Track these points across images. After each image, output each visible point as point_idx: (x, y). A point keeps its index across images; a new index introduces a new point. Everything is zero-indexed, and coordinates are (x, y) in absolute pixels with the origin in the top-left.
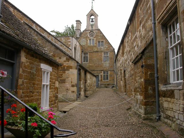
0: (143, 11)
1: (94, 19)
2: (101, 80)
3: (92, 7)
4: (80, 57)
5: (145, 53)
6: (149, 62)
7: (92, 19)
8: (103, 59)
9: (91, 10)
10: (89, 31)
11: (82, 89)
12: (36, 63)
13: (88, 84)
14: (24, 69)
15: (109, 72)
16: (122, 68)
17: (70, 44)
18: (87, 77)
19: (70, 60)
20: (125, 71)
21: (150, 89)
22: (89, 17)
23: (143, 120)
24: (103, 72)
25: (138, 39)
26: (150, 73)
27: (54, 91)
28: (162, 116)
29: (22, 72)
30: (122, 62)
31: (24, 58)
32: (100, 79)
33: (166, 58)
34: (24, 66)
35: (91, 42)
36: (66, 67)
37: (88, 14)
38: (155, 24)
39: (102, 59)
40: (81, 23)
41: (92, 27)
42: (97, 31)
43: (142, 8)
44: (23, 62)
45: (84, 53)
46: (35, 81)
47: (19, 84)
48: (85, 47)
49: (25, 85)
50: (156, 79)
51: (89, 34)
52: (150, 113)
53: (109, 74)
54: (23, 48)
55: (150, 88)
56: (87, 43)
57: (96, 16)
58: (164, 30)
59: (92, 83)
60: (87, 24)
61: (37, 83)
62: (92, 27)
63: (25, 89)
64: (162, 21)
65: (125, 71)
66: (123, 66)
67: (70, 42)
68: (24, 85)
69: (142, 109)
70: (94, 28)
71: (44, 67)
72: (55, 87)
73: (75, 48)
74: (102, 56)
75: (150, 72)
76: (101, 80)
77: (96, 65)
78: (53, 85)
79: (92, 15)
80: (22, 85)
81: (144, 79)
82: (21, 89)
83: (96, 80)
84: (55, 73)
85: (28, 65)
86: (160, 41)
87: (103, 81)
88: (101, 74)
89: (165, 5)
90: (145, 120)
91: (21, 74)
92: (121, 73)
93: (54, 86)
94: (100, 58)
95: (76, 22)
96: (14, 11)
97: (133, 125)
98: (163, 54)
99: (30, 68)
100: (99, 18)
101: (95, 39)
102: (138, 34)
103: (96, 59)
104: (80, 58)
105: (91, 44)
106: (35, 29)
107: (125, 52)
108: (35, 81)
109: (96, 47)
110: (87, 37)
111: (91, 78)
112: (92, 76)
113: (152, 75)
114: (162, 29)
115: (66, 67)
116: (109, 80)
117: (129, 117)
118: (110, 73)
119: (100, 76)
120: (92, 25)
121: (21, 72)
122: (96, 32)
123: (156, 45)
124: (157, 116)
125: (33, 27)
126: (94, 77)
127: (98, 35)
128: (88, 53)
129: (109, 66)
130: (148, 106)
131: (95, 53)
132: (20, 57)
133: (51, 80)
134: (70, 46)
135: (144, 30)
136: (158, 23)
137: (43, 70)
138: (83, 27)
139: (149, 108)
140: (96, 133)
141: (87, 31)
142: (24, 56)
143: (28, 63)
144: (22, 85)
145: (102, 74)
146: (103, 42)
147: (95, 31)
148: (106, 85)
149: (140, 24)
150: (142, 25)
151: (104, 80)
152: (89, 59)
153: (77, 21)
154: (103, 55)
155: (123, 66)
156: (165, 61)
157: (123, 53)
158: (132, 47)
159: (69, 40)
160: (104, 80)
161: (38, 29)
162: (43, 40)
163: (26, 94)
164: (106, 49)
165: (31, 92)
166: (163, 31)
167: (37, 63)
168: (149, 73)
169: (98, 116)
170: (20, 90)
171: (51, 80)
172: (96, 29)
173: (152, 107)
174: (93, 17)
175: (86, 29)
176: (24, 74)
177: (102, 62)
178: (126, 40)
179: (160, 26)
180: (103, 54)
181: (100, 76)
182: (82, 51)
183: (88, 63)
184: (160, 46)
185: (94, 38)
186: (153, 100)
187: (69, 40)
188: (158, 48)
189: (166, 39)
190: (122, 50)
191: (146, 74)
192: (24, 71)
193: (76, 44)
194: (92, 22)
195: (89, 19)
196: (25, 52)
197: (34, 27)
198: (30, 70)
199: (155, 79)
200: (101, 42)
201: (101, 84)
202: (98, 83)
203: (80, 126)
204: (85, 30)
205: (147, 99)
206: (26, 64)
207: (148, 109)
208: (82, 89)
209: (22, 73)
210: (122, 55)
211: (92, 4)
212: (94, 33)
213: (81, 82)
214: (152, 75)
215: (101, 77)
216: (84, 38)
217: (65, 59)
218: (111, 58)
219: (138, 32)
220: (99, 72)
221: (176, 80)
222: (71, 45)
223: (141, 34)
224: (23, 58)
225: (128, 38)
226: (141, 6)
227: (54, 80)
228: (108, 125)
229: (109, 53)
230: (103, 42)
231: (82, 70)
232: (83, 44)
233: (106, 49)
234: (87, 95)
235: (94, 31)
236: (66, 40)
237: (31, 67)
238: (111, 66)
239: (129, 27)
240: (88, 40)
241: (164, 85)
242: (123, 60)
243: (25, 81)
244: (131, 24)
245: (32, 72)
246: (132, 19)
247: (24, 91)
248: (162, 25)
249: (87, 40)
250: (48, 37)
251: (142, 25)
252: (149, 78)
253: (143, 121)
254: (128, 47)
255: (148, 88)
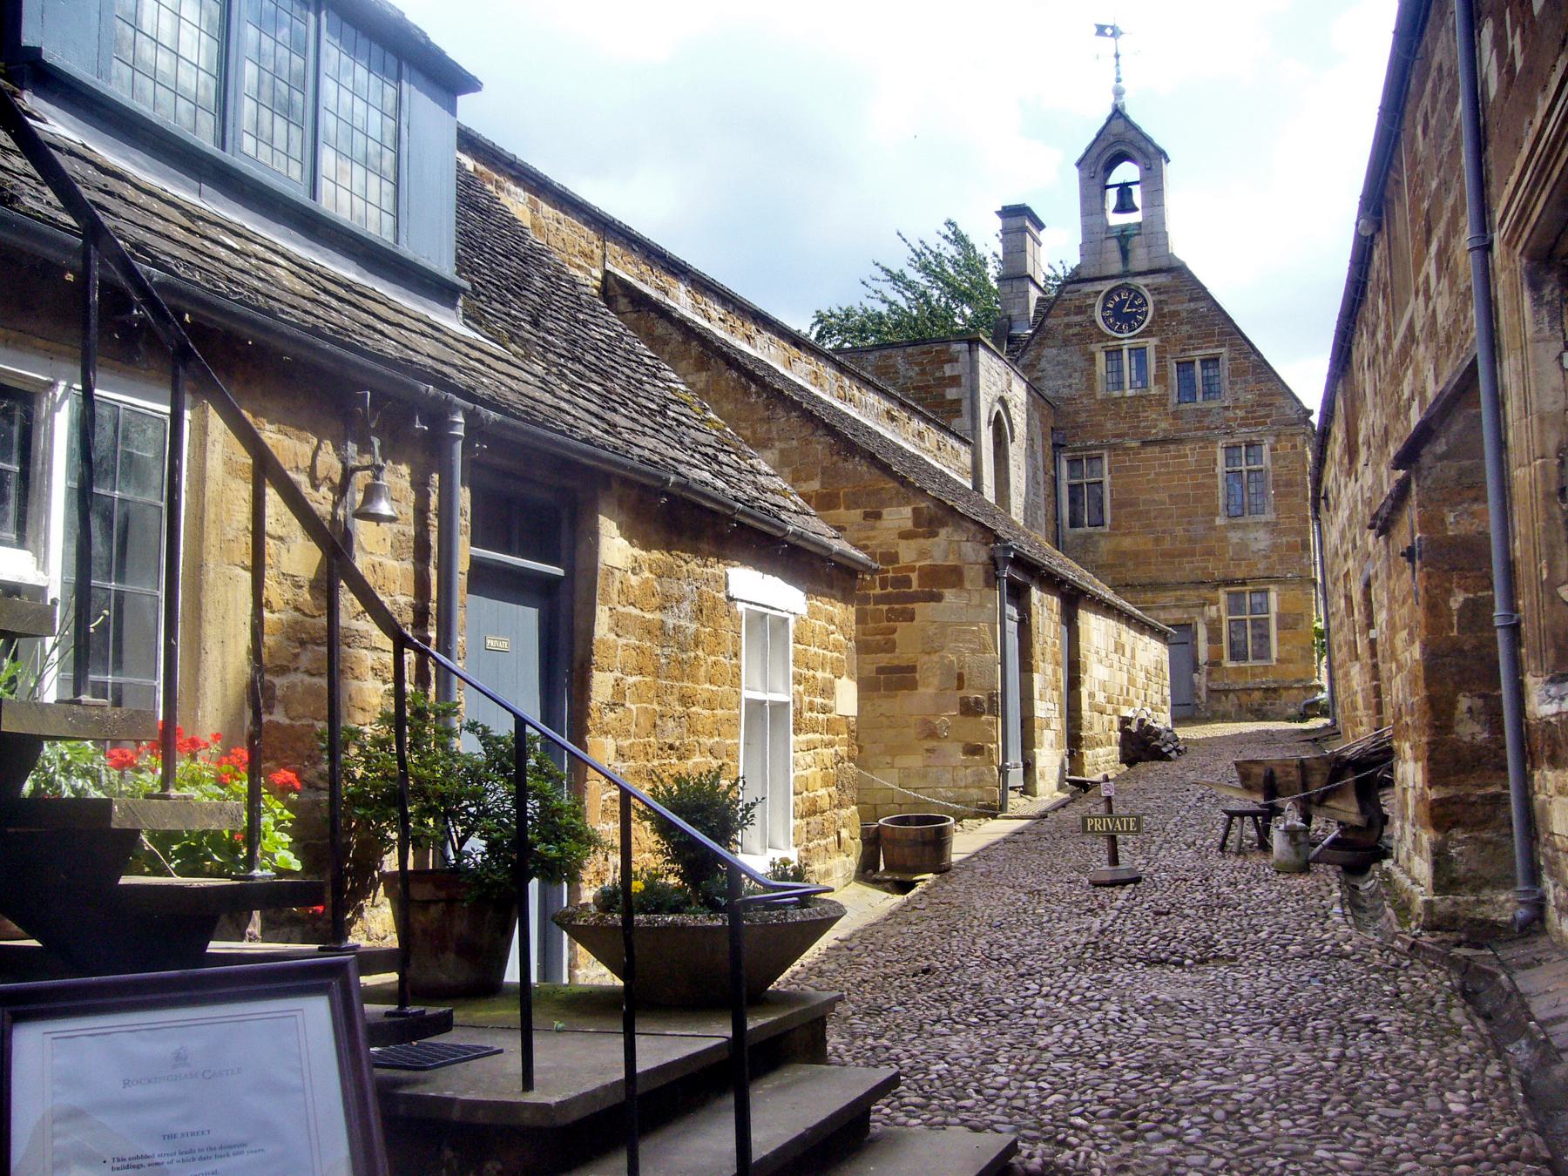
0: (1438, 147)
1: (1136, 191)
2: (1215, 663)
3: (1119, 80)
4: (1042, 492)
5: (1426, 459)
6: (1455, 523)
7: (1124, 189)
8: (1221, 493)
9: (1110, 120)
10: (1098, 286)
11: (1048, 727)
12: (692, 565)
13: (1091, 695)
14: (620, 608)
15: (1273, 596)
16: (1350, 563)
17: (959, 401)
18: (1089, 641)
19: (944, 525)
20: (1368, 585)
21: (1470, 710)
22: (1101, 174)
23: (1424, 928)
24: (1222, 595)
25: (1422, 348)
26: (1466, 600)
27: (830, 744)
28: (1551, 896)
29: (611, 630)
30: (1350, 518)
31: (622, 543)
32: (1203, 656)
33: (1562, 491)
34: (621, 592)
35: (1120, 371)
36: (914, 576)
37: (1088, 150)
38: (1488, 248)
39: (1213, 497)
40: (1040, 226)
41: (1125, 254)
42: (1160, 279)
43: (1433, 122)
44: (611, 570)
45: (1071, 462)
46: (693, 678)
47: (593, 704)
48: (1077, 413)
49: (633, 707)
50: (1501, 637)
51: (1105, 308)
52: (1478, 883)
53: (1274, 607)
54: (608, 486)
55: (1464, 703)
56: (1090, 376)
57: (1151, 157)
58: (1547, 291)
59: (1132, 682)
60: (1087, 231)
61: (705, 695)
62: (1125, 254)
63: (633, 729)
64: (1525, 235)
65: (1368, 585)
66: (1354, 546)
67: (955, 381)
68: (628, 704)
69: (1425, 855)
70: (1139, 260)
71: (753, 586)
72: (832, 715)
73: (997, 424)
74: (1215, 476)
75: (1466, 590)
76: (1215, 663)
77: (1167, 544)
78: (818, 700)
79: (1120, 158)
80: (612, 706)
81: (1425, 646)
82: (606, 733)
83: (1166, 657)
84: (831, 621)
85: (647, 580)
86: (1523, 373)
87: (1233, 664)
88: (1212, 611)
89: (1526, 124)
90: (1438, 928)
91: (603, 642)
92: (1348, 598)
93: (825, 710)
94: (1198, 486)
95: (997, 224)
96: (534, 210)
97: (1341, 957)
98: (1543, 466)
99: (656, 601)
100: (1171, 174)
101: (1151, 343)
102: (1415, 308)
103: (1164, 496)
104: (1041, 501)
105: (1119, 385)
106: (688, 314)
107: (1360, 440)
108: (693, 678)
109: (1161, 401)
110: (1088, 334)
111: (1119, 648)
112: (1129, 635)
113: (1477, 612)
114: (1535, 286)
115: (914, 576)
116: (1274, 655)
117: (1337, 909)
118: (1281, 603)
119: (1202, 633)
120: (1124, 237)
121: (606, 627)
122: (1156, 290)
123: (1498, 403)
124: (1522, 903)
125: (677, 300)
126: (1146, 639)
127: (1175, 314)
128: (1100, 458)
129: (1275, 547)
130: (1458, 834)
131: (1157, 449)
132: (595, 533)
133: (804, 671)
134: (958, 413)
135: (1445, 282)
136: (1504, 248)
137: (741, 607)
138: (1057, 251)
139: (1461, 842)
140: (1074, 999)
141: (1088, 288)
142: (615, 532)
143: (647, 574)
144: (612, 706)
145: (1219, 609)
146: (1215, 360)
147: (1149, 280)
148: (1257, 695)
149: (1428, 243)
150: (1433, 248)
151: (1233, 657)
152: (1117, 505)
153: (1009, 213)
154: (1221, 468)
155: (1354, 546)
156: (1556, 509)
157: (1351, 450)
158: (1397, 407)
159: (948, 370)
160: (1233, 657)
161: (714, 315)
162: (746, 390)
163: (641, 762)
164: (1240, 413)
165: (671, 747)
166: (1538, 301)
167: (699, 570)
168: (1457, 601)
169: (1119, 904)
170: (602, 739)
171: (804, 671)
172: (1156, 265)
173: (1486, 835)
174: (1126, 172)
175: (1076, 271)
176: (621, 641)
177: (1219, 521)
178: (1363, 348)
179: (1521, 263)
180: (1220, 456)
181: (1202, 633)
182: (1057, 446)
183: (1107, 530)
184: (1526, 409)
185: (1147, 333)
186: (1491, 790)
187: (948, 370)
188: (1509, 420)
189: (1560, 358)
190: (1343, 426)
191: (1434, 607)
192: (618, 626)
193: (1007, 396)
194: (1125, 206)
195: (1098, 190)
196: (621, 506)
197: (681, 300)
198: (657, 615)
199: (1494, 640)
200: (1202, 361)
201: (1211, 691)
202: (1192, 684)
203: (987, 961)
204: (1075, 279)
205: (1446, 785)
206: (634, 580)
207: (1460, 854)
208: (1048, 727)
209: (613, 636)
210: (1346, 461)
211: (1121, 68)
212: (1139, 295)
213: (1036, 676)
214: (1477, 612)
215: (1214, 637)
216: (1066, 342)
217: (899, 516)
218: (1286, 486)
219: (1421, 298)
220: (1191, 596)
221: (146, 681)
222: (966, 405)
223: (1434, 311)
224: (615, 547)
225: (1374, 334)
226: (1426, 101)
227: (824, 670)
228: (1173, 953)
229: (1266, 449)
230: (1215, 360)
231: (1036, 594)
232: (1065, 392)
233: (1240, 413)
234: (1087, 769)
235: (1139, 282)
236: (923, 372)
237: (666, 597)
238: (1291, 547)
239: (1371, 248)
240: (1101, 358)
241: (1552, 681)
242: (1356, 502)
243: (631, 680)
244: (1379, 229)
245: (670, 622)
246: (1388, 195)
247: (626, 743)
248: (1531, 259)
249: (1091, 359)
250: (789, 363)
251: (1433, 248)
252: (1455, 633)
253: (1426, 938)
254: (1375, 406)
255: (1453, 704)
